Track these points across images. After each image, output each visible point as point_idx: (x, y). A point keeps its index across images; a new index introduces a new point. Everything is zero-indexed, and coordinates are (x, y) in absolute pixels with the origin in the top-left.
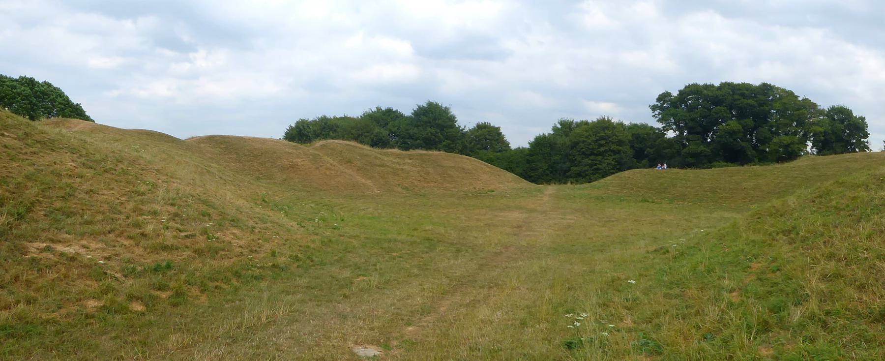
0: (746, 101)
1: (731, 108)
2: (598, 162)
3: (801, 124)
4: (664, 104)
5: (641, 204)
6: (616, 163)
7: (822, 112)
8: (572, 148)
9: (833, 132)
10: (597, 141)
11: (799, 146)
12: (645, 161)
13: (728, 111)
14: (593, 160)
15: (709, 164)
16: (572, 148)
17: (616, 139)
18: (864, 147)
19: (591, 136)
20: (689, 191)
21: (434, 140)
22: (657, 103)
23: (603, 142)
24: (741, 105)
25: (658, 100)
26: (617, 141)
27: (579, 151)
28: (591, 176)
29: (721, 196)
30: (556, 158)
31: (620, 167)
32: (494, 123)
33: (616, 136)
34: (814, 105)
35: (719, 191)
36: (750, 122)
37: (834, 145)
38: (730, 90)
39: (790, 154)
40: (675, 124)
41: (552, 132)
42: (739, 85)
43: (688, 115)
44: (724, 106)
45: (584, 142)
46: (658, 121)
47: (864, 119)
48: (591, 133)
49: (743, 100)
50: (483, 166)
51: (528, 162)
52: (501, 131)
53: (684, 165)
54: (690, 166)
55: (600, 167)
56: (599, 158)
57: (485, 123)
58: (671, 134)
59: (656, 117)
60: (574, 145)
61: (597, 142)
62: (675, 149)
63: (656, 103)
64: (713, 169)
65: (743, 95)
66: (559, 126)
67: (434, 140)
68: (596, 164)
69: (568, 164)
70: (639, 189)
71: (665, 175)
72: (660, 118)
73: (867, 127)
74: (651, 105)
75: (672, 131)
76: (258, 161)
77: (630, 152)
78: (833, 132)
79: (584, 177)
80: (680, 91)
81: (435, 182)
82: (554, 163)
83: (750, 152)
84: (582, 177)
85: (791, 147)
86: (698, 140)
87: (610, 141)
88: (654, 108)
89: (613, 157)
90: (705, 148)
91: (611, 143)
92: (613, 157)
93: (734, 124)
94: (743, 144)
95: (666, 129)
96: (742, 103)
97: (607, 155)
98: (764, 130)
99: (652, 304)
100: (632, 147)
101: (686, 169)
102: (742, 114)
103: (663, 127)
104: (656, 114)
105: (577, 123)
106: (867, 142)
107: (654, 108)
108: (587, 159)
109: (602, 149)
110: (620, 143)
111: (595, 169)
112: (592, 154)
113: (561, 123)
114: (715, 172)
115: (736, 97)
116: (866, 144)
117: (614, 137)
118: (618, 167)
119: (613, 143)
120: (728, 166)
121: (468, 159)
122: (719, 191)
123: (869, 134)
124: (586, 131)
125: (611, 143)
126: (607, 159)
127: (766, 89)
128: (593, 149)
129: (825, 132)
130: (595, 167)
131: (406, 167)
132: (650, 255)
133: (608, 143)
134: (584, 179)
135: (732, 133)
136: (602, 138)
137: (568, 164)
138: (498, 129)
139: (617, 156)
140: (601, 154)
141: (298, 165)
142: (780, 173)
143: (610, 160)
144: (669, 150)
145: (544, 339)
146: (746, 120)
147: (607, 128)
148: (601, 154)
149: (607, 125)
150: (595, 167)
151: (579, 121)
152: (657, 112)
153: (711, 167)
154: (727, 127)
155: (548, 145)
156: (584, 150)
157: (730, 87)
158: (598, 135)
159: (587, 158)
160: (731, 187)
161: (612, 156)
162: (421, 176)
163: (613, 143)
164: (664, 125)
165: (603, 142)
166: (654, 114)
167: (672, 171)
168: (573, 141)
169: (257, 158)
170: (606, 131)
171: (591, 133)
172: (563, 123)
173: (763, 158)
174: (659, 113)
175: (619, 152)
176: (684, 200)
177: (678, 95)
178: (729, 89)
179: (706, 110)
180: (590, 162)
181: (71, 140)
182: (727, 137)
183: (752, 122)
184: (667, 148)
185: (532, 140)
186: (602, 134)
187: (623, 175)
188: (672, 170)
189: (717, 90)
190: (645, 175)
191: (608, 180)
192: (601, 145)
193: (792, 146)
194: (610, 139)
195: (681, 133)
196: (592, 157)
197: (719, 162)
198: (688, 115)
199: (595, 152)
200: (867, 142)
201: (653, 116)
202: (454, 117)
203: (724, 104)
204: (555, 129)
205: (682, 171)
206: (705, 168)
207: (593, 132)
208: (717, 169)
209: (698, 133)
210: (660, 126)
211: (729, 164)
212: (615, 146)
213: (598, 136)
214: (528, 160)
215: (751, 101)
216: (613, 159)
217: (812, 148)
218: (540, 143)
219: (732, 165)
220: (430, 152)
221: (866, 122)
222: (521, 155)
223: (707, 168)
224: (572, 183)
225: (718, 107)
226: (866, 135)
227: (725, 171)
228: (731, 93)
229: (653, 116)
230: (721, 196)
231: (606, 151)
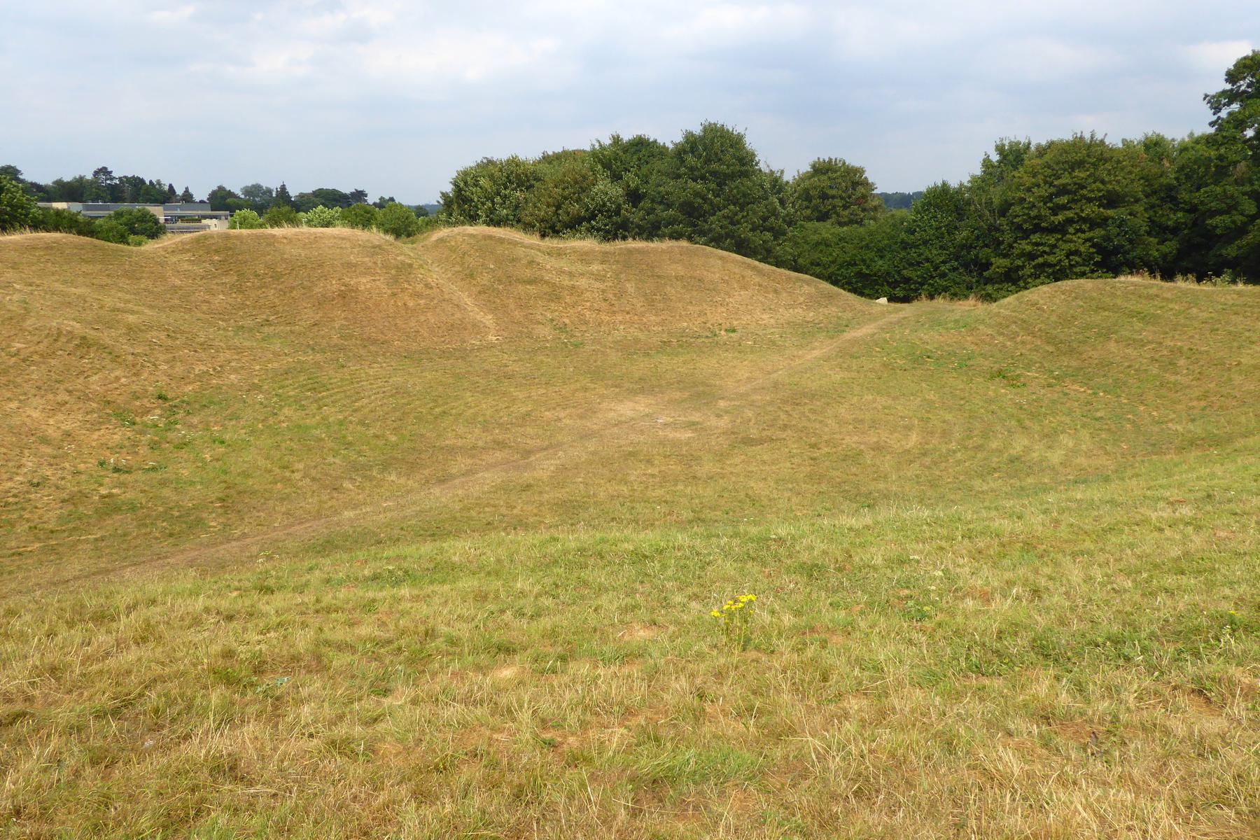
2: (1047, 249)
6: (1092, 250)
10: (1050, 198)
14: (1037, 244)
19: (1038, 186)
21: (700, 206)
23: (1064, 200)
28: (1029, 280)
33: (1103, 182)
45: (1023, 200)
50: (749, 273)
51: (905, 246)
57: (831, 159)
61: (1051, 200)
62: (1242, 214)
66: (995, 158)
67: (700, 206)
76: (279, 287)
80: (944, 184)
81: (628, 313)
89: (1088, 235)
92: (1088, 235)
99: (1134, 757)
105: (1038, 147)
112: (1037, 229)
113: (1000, 149)
119: (1090, 200)
121: (721, 258)
126: (1071, 241)
128: (1038, 217)
130: (1040, 260)
131: (582, 283)
132: (933, 625)
136: (1063, 191)
139: (1098, 233)
141: (357, 290)
145: (1114, 722)
151: (1044, 143)
158: (1056, 183)
161: (1084, 232)
162: (605, 300)
163: (1090, 200)
165: (1064, 200)
169: (278, 280)
175: (1103, 222)
180: (1029, 248)
186: (1065, 180)
187: (821, 286)
191: (1120, 282)
192: (1056, 210)
194: (1084, 192)
196: (1035, 238)
202: (753, 155)
213: (1054, 186)
216: (1086, 240)
220: (651, 245)
231: (1070, 221)
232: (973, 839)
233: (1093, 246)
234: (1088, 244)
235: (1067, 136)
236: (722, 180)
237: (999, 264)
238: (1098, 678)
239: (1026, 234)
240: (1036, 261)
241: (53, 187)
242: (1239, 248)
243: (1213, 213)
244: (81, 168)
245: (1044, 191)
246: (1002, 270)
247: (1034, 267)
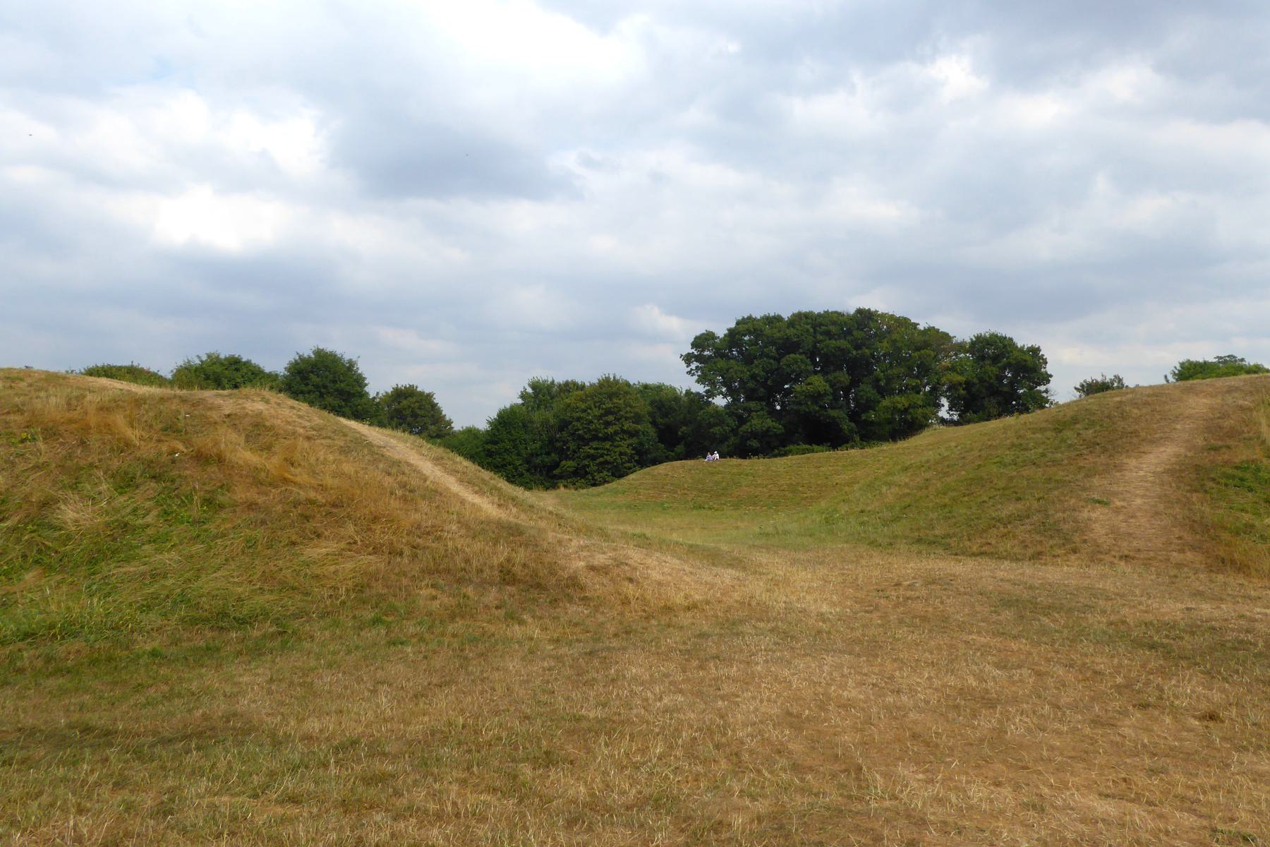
0: (833, 343)
1: (812, 356)
2: (605, 452)
3: (925, 370)
4: (703, 351)
5: (695, 512)
6: (633, 452)
7: (961, 347)
8: (561, 429)
9: (981, 380)
10: (600, 417)
11: (925, 410)
12: (680, 448)
13: (808, 361)
14: (596, 449)
15: (783, 449)
16: (561, 429)
17: (631, 412)
18: (1040, 402)
19: (591, 409)
20: (761, 492)
22: (693, 350)
23: (611, 418)
24: (825, 350)
25: (694, 345)
26: (632, 415)
27: (573, 434)
29: (805, 495)
30: (534, 446)
31: (644, 459)
32: (423, 387)
33: (631, 406)
34: (946, 337)
35: (801, 489)
36: (843, 377)
37: (986, 402)
38: (809, 327)
39: (906, 427)
40: (724, 384)
41: (520, 401)
42: (819, 315)
43: (745, 370)
44: (801, 354)
45: (578, 419)
46: (698, 381)
47: (1038, 349)
48: (591, 403)
49: (828, 342)
52: (435, 401)
53: (743, 452)
54: (755, 453)
55: (608, 458)
56: (607, 445)
58: (720, 401)
59: (693, 375)
60: (564, 425)
63: (691, 351)
64: (790, 457)
65: (828, 334)
66: (530, 390)
68: (602, 456)
69: (554, 456)
70: (686, 491)
71: (721, 469)
72: (699, 376)
73: (1046, 363)
74: (684, 354)
75: (721, 396)
77: (652, 432)
78: (981, 380)
79: (583, 477)
82: (532, 455)
83: (847, 425)
84: (583, 476)
85: (910, 413)
86: (762, 409)
87: (622, 416)
88: (688, 359)
90: (774, 423)
91: (623, 419)
93: (818, 382)
94: (833, 413)
95: (710, 394)
96: (827, 346)
97: (618, 439)
98: (867, 390)
100: (654, 423)
101: (750, 458)
102: (829, 363)
103: (707, 392)
104: (692, 370)
106: (1046, 391)
107: (688, 359)
108: (587, 447)
109: (610, 430)
110: (637, 419)
111: (601, 463)
112: (596, 438)
114: (794, 462)
115: (820, 337)
116: (1044, 395)
117: (628, 409)
118: (637, 458)
120: (813, 451)
122: (801, 489)
123: (1051, 376)
124: (582, 400)
125: (623, 419)
127: (865, 317)
128: (596, 430)
129: (967, 383)
130: (601, 459)
133: (618, 420)
134: (583, 480)
135: (817, 397)
137: (554, 456)
138: (430, 396)
139: (634, 440)
140: (607, 438)
142: (887, 459)
143: (625, 446)
144: (719, 428)
146: (837, 374)
147: (611, 396)
148: (607, 438)
149: (614, 389)
150: (601, 459)
152: (693, 366)
153: (785, 454)
154: (809, 387)
155: (520, 424)
156: (580, 432)
157: (809, 321)
159: (587, 444)
160: (819, 483)
161: (625, 440)
163: (626, 419)
164: (707, 388)
165: (611, 418)
166: (689, 369)
167: (731, 463)
168: (562, 417)
170: (615, 400)
171: (591, 403)
172: (535, 386)
173: (870, 434)
174: (697, 367)
176: (755, 504)
177: (725, 335)
178: (808, 324)
179: (772, 361)
181: (82, 451)
182: (809, 403)
183: (847, 376)
184: (718, 425)
185: (494, 415)
187: (656, 472)
188: (654, 470)
189: (788, 327)
190: (690, 470)
192: (608, 424)
193: (911, 410)
195: (735, 400)
196: (595, 444)
197: (798, 445)
198: (745, 370)
199: (600, 435)
200: (1046, 391)
201: (689, 373)
203: (801, 351)
204: (524, 396)
205: (746, 462)
206: (775, 456)
207: (595, 402)
208: (795, 457)
209: (760, 399)
210: (700, 389)
211: (815, 447)
212: (631, 424)
214: (489, 450)
215: (843, 343)
217: (950, 409)
218: (506, 421)
219: (820, 448)
221: (1043, 355)
222: (476, 442)
223: (782, 455)
224: (565, 487)
225: (792, 355)
226: (1046, 379)
227: (809, 458)
228: (812, 330)
229: (689, 373)
230: (805, 495)
231: (616, 433)
232: (182, 845)
233: (633, 449)
234: (631, 448)
235: (588, 375)
236: (995, 359)
237: (569, 464)
238: (536, 728)
239: (586, 442)
240: (598, 461)
241: (343, 365)
242: (728, 446)
243: (711, 425)
244: (127, 363)
245: (597, 412)
246: (571, 470)
247: (597, 465)
